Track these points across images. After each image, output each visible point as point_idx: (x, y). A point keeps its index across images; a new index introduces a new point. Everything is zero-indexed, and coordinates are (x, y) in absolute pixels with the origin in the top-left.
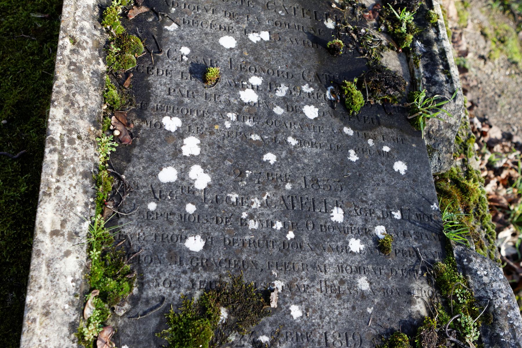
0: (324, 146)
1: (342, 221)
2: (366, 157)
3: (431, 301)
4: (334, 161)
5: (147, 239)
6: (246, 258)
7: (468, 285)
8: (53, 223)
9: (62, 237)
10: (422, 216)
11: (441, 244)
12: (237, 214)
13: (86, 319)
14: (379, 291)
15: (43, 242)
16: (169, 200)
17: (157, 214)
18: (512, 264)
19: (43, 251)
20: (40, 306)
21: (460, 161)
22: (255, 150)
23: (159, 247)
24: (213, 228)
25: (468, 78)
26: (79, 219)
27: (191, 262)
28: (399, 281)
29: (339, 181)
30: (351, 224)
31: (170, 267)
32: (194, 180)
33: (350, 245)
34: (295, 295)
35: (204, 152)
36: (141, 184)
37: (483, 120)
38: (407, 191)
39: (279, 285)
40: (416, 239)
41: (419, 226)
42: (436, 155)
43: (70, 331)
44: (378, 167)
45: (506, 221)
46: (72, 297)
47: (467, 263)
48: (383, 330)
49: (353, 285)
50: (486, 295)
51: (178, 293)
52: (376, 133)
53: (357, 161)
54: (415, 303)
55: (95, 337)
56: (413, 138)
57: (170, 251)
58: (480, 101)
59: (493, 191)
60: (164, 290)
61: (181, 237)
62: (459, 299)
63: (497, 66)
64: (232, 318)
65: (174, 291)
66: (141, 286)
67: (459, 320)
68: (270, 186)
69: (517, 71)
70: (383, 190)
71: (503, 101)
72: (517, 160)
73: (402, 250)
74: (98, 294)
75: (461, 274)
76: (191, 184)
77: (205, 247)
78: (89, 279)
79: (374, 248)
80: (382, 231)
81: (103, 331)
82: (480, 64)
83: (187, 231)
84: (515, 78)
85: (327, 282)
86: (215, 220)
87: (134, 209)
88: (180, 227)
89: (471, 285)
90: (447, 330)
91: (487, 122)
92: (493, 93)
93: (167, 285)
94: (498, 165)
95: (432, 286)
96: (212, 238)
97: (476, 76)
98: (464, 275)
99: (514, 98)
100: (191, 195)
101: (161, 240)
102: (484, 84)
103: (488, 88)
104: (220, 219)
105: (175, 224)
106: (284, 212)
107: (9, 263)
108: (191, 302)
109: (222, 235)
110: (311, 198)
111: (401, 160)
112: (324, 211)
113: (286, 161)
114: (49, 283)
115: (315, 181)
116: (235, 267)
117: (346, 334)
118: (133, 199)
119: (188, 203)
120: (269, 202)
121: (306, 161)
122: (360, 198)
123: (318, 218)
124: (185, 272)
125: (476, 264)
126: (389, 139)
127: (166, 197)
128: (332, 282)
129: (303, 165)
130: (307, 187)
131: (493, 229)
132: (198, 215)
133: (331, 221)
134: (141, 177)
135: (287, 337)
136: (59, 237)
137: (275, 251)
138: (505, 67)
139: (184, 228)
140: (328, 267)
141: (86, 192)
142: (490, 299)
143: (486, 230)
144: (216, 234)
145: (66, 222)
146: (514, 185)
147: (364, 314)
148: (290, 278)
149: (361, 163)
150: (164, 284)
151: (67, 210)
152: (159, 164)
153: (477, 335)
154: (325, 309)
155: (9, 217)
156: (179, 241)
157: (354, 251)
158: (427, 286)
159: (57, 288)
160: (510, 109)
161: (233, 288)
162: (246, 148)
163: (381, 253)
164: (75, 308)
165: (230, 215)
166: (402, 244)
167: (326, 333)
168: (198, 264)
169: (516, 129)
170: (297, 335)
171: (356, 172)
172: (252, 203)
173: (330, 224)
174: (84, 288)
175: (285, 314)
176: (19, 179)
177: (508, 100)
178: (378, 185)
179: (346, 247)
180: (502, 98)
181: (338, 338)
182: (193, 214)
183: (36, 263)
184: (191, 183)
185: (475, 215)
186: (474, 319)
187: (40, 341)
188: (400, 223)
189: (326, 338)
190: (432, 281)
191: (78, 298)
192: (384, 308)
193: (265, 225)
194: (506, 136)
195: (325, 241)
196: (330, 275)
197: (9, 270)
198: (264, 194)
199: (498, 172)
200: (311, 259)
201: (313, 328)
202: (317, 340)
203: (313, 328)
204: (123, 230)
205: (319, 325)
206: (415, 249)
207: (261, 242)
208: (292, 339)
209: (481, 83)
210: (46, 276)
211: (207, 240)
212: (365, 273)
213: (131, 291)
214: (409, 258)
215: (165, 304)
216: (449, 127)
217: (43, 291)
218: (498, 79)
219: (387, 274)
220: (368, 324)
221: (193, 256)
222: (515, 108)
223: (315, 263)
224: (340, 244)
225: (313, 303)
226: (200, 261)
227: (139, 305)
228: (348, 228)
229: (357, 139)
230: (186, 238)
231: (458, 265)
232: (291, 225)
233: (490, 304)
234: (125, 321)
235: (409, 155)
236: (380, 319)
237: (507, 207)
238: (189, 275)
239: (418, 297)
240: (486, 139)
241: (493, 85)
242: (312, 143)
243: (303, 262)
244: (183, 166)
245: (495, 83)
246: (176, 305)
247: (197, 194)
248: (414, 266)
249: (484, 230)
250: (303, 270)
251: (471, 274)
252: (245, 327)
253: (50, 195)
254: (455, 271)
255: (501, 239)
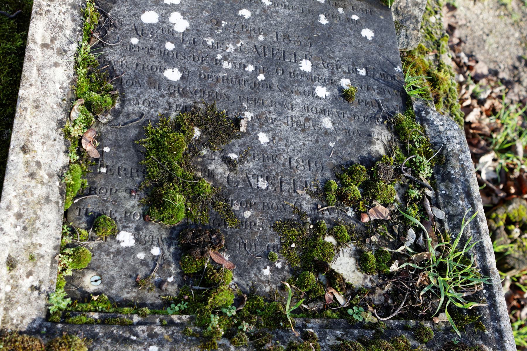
0: (296, 9)
1: (310, 71)
2: (335, 22)
3: (390, 144)
4: (305, 22)
5: (129, 66)
6: (219, 91)
7: (425, 132)
8: (44, 37)
9: (52, 50)
10: (386, 76)
11: (403, 100)
12: (212, 55)
13: (72, 120)
14: (342, 131)
15: (34, 50)
16: (150, 38)
17: (139, 47)
18: (491, 185)
19: (34, 58)
20: (31, 100)
21: (432, 55)
22: (232, 6)
23: (140, 74)
24: (190, 64)
25: (457, 17)
26: (67, 40)
27: (169, 89)
28: (361, 125)
29: (309, 39)
30: (318, 75)
31: (149, 90)
32: (174, 24)
33: (316, 91)
34: (263, 125)
35: (183, 2)
36: (125, 22)
37: (470, 56)
38: (372, 53)
39: (249, 115)
40: (378, 94)
41: (382, 83)
42: (403, 31)
43: (57, 126)
44: (346, 31)
45: (488, 148)
46: (60, 100)
47: (425, 115)
48: (343, 162)
49: (317, 123)
50: (440, 141)
51: (156, 111)
52: (346, 3)
53: (326, 24)
54: (375, 144)
55: (80, 136)
56: (381, 11)
57: (149, 78)
58: (468, 38)
59: (477, 119)
60: (143, 108)
61: (160, 68)
62: (416, 143)
63: (487, 7)
64: (204, 136)
65: (153, 110)
66: (123, 103)
67: (414, 159)
68: (244, 36)
69: (507, 13)
70: (350, 50)
71: (491, 40)
72: (501, 94)
73: (366, 101)
74: (83, 102)
75: (419, 123)
76: (171, 27)
77: (182, 78)
78: (76, 90)
79: (338, 97)
80: (347, 84)
81: (87, 132)
82: (469, 4)
83: (165, 64)
84: (504, 19)
85: (294, 118)
86: (192, 58)
87: (118, 42)
88: (160, 60)
89: (428, 133)
90: (403, 167)
91: (474, 58)
92: (481, 33)
93: (146, 105)
94: (483, 96)
95: (391, 132)
96: (188, 71)
97: (465, 15)
98: (422, 124)
99: (502, 38)
100: (171, 35)
101: (142, 68)
102: (473, 23)
103: (477, 27)
104: (197, 58)
105: (155, 57)
106: (256, 58)
107: (5, 104)
108: (167, 120)
109: (198, 70)
110: (281, 50)
111: (369, 28)
112: (293, 61)
113: (260, 17)
114: (39, 84)
115: (286, 36)
116: (209, 97)
117: (309, 161)
118: (117, 33)
119: (168, 41)
120: (242, 49)
121: (279, 19)
122: (328, 54)
123: (287, 66)
124: (163, 96)
125: (433, 116)
126: (358, 10)
127: (147, 35)
128: (298, 118)
129: (275, 22)
130: (279, 40)
131: (461, 116)
132: (177, 53)
133: (299, 70)
134: (125, 17)
135: (254, 157)
136: (49, 49)
137: (247, 88)
138: (495, 8)
139: (163, 61)
140: (295, 106)
141: (74, 20)
142: (444, 144)
143: (454, 116)
144: (193, 69)
145: (56, 39)
146: (497, 116)
147: (326, 147)
148: (259, 111)
149: (331, 26)
150: (143, 103)
151: (57, 30)
152: (142, 8)
153: (430, 173)
154: (291, 139)
155: (6, 65)
156: (158, 70)
157: (320, 96)
158: (387, 132)
159: (47, 89)
160: (498, 48)
161: (206, 113)
162: (223, 3)
163: (345, 101)
164: (62, 110)
165: (206, 55)
166: (365, 95)
167: (290, 158)
168: (175, 91)
169: (502, 67)
170: (264, 156)
171: (325, 33)
172: (227, 48)
173: (298, 72)
174: (70, 96)
175: (253, 139)
176: (15, 35)
177: (497, 39)
178: (346, 46)
179: (312, 92)
180: (490, 37)
181: (301, 163)
182: (172, 51)
183: (28, 66)
184: (171, 27)
185: (444, 103)
186: (427, 158)
187: (31, 127)
188: (364, 78)
189: (290, 162)
190: (391, 129)
191: (66, 102)
192: (345, 145)
193: (238, 66)
194: (493, 73)
195: (293, 85)
196: (296, 112)
197: (5, 111)
198: (238, 42)
199: (481, 103)
200: (279, 98)
201: (278, 152)
202: (282, 162)
203: (278, 152)
204: (107, 57)
205: (284, 151)
206: (377, 101)
207: (234, 80)
208: (259, 159)
209: (470, 22)
210: (37, 78)
211: (184, 72)
212: (329, 115)
213: (113, 105)
214: (371, 108)
215: (143, 119)
216: (416, 5)
217: (33, 89)
218: (487, 19)
219: (350, 119)
220: (330, 155)
221: (170, 84)
222: (503, 47)
223: (283, 102)
224: (307, 89)
225: (279, 133)
226: (177, 89)
227: (121, 117)
228: (315, 77)
229: (328, 6)
230: (165, 69)
231: (416, 117)
232: (262, 69)
233: (443, 148)
234: (107, 128)
235: (376, 24)
236: (341, 153)
237: (489, 135)
238: (166, 98)
239: (378, 139)
240: (472, 74)
241: (482, 25)
242: (285, 5)
243: (272, 100)
244: (164, 12)
245: (484, 23)
246: (154, 121)
247: (176, 35)
248: (376, 115)
249: (452, 116)
250: (272, 106)
251: (428, 124)
252: (216, 145)
253: (41, 14)
254: (414, 121)
255: (482, 163)
